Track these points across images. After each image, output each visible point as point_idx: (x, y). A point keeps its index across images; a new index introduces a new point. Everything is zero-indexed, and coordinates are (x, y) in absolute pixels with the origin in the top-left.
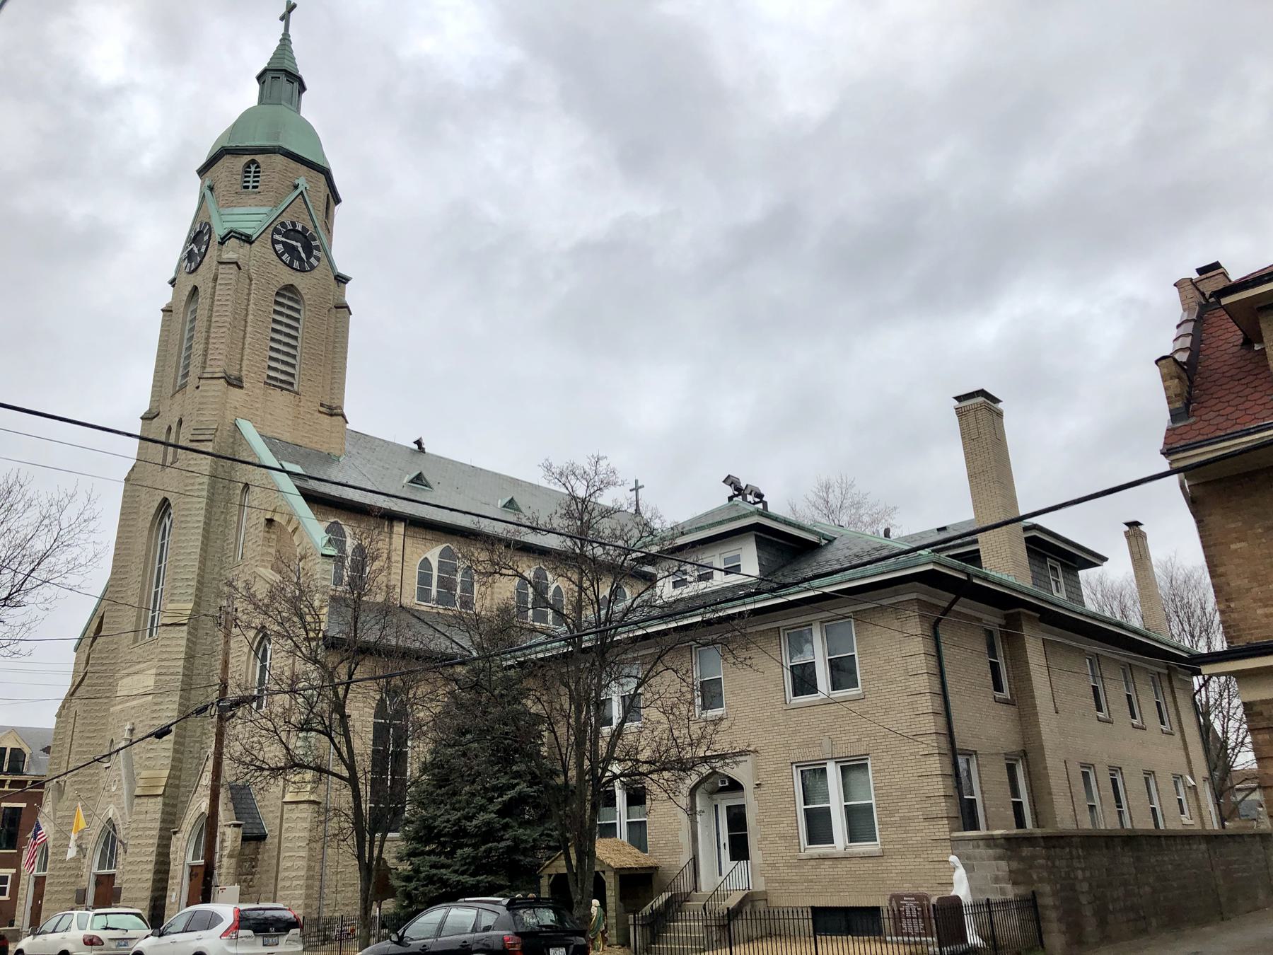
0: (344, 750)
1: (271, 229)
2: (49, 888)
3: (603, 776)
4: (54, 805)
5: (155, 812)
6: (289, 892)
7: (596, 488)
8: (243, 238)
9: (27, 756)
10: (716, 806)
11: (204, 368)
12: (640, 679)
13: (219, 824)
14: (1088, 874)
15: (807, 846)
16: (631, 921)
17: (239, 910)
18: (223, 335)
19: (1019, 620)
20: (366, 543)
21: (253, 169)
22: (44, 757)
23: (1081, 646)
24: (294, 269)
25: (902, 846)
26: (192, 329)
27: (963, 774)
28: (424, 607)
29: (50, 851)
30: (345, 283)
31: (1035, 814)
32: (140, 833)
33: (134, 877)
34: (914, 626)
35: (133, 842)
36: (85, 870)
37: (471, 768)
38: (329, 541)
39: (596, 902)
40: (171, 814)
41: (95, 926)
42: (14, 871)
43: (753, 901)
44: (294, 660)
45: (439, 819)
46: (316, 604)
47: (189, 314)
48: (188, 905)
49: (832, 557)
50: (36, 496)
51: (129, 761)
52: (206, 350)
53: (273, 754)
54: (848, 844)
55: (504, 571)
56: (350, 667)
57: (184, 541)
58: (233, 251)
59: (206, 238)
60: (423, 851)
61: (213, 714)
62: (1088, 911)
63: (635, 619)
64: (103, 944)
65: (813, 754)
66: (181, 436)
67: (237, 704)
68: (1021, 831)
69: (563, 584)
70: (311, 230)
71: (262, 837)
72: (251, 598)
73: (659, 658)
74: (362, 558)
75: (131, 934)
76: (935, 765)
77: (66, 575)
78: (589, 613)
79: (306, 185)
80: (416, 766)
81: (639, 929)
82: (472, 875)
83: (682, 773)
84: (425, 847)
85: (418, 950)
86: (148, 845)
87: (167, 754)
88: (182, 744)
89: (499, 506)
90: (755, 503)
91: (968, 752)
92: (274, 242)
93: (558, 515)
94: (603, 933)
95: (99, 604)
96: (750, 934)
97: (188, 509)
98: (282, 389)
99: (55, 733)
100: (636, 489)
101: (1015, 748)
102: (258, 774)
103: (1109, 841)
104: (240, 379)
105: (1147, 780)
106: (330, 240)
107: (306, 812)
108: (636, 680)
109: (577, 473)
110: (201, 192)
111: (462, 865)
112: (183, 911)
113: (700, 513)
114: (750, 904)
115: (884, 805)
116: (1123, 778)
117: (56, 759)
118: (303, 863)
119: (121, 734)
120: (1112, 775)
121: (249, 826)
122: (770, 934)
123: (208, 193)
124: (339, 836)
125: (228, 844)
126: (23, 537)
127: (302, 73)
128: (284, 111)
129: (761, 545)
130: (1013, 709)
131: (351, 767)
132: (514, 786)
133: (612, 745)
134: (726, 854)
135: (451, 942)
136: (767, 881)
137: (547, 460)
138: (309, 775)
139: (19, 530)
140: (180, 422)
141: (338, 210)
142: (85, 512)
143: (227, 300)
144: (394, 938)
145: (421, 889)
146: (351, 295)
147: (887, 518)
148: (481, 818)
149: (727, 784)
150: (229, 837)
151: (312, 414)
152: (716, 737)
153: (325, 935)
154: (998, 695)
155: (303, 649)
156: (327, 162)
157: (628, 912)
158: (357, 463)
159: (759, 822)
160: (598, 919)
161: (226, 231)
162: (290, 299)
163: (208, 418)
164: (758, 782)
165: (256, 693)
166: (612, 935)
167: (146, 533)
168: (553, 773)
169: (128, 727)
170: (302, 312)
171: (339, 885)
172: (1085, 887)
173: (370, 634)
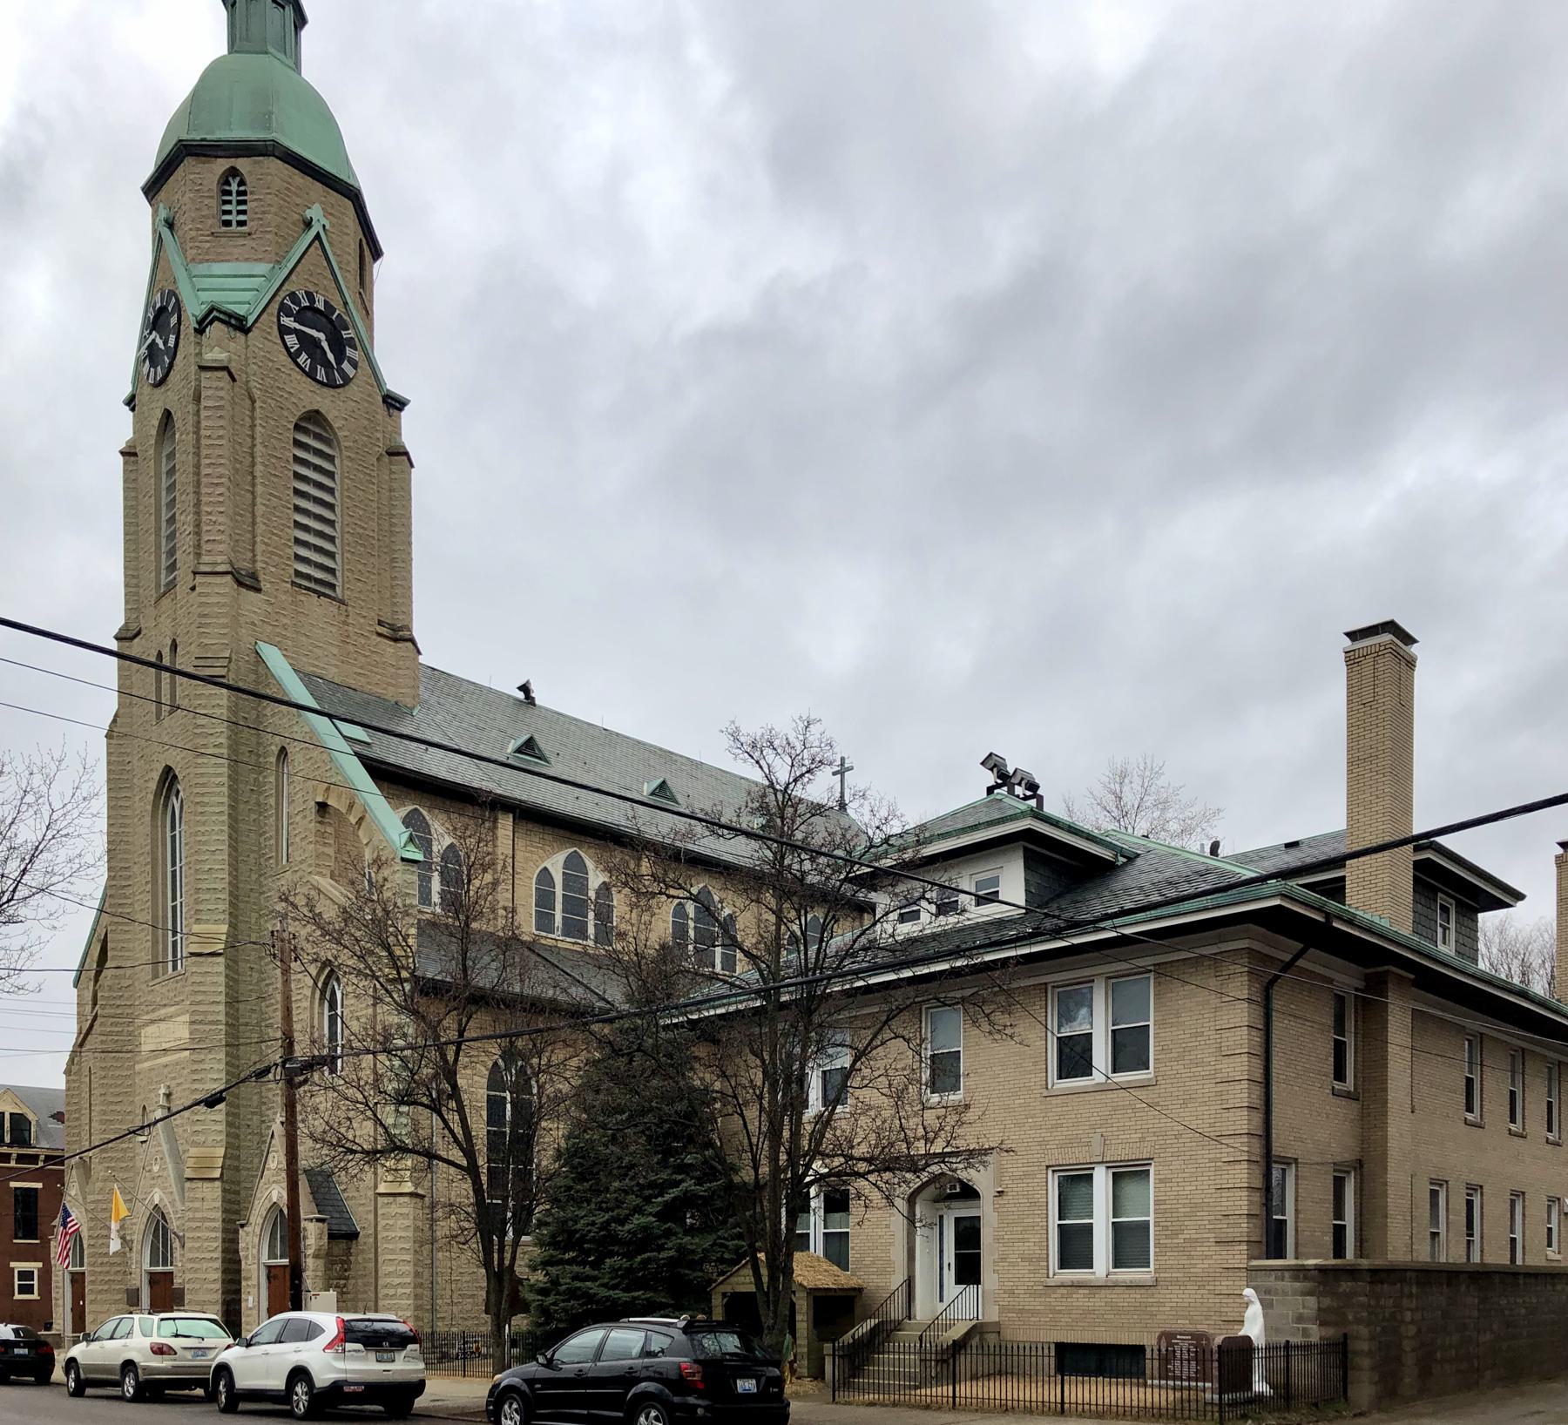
1: (275, 306)
2: (90, 1287)
3: (805, 1174)
4: (82, 1189)
7: (804, 769)
8: (233, 321)
9: (33, 1123)
10: (941, 1217)
11: (198, 555)
14: (1418, 1316)
15: (1057, 1271)
18: (221, 499)
19: (1386, 983)
21: (234, 187)
22: (54, 1125)
23: (1457, 1020)
25: (1182, 1275)
27: (1276, 1191)
30: (400, 410)
31: (1361, 1242)
32: (199, 1224)
34: (1240, 986)
35: (191, 1235)
36: (134, 1267)
38: (411, 839)
40: (233, 1203)
41: (162, 1333)
42: (40, 1265)
43: (982, 1333)
45: (582, 1221)
47: (164, 460)
48: (271, 1313)
49: (1134, 885)
51: (172, 1138)
53: (364, 1132)
54: (1111, 1270)
55: (672, 892)
57: (203, 834)
58: (219, 346)
59: (174, 320)
62: (1409, 1360)
63: (855, 966)
64: (176, 1354)
65: (1075, 1156)
67: (311, 1065)
68: (1338, 1261)
70: (336, 303)
71: (354, 1236)
72: (316, 919)
73: (886, 1022)
75: (207, 1343)
76: (1242, 1175)
77: (72, 879)
79: (324, 221)
82: (624, 1290)
85: (573, 1376)
88: (236, 1115)
89: (645, 794)
90: (1026, 798)
91: (1285, 1160)
92: (283, 330)
94: (791, 1363)
95: (97, 921)
97: (203, 785)
98: (320, 594)
101: (1348, 1157)
103: (1451, 1276)
104: (254, 576)
105: (1513, 1203)
106: (370, 328)
109: (776, 743)
110: (154, 231)
111: (612, 1279)
114: (978, 1337)
115: (1166, 1224)
116: (1482, 1199)
118: (409, 1268)
119: (155, 1100)
120: (1468, 1195)
121: (334, 1221)
122: (1000, 1371)
123: (166, 232)
128: (271, 64)
129: (1031, 862)
130: (1355, 1105)
131: (469, 1153)
132: (677, 1184)
134: (950, 1276)
135: (610, 1368)
136: (1002, 1310)
137: (733, 722)
140: (174, 646)
141: (381, 271)
142: (83, 786)
143: (220, 437)
145: (562, 1304)
146: (412, 430)
147: (1204, 825)
149: (958, 1190)
150: (313, 1235)
154: (1338, 1085)
155: (395, 996)
156: (354, 175)
157: (822, 1339)
159: (997, 1239)
161: (205, 308)
162: (317, 437)
164: (1000, 1189)
166: (803, 1366)
167: (148, 818)
169: (162, 1091)
170: (337, 461)
171: (454, 1296)
172: (1412, 1330)
173: (486, 976)
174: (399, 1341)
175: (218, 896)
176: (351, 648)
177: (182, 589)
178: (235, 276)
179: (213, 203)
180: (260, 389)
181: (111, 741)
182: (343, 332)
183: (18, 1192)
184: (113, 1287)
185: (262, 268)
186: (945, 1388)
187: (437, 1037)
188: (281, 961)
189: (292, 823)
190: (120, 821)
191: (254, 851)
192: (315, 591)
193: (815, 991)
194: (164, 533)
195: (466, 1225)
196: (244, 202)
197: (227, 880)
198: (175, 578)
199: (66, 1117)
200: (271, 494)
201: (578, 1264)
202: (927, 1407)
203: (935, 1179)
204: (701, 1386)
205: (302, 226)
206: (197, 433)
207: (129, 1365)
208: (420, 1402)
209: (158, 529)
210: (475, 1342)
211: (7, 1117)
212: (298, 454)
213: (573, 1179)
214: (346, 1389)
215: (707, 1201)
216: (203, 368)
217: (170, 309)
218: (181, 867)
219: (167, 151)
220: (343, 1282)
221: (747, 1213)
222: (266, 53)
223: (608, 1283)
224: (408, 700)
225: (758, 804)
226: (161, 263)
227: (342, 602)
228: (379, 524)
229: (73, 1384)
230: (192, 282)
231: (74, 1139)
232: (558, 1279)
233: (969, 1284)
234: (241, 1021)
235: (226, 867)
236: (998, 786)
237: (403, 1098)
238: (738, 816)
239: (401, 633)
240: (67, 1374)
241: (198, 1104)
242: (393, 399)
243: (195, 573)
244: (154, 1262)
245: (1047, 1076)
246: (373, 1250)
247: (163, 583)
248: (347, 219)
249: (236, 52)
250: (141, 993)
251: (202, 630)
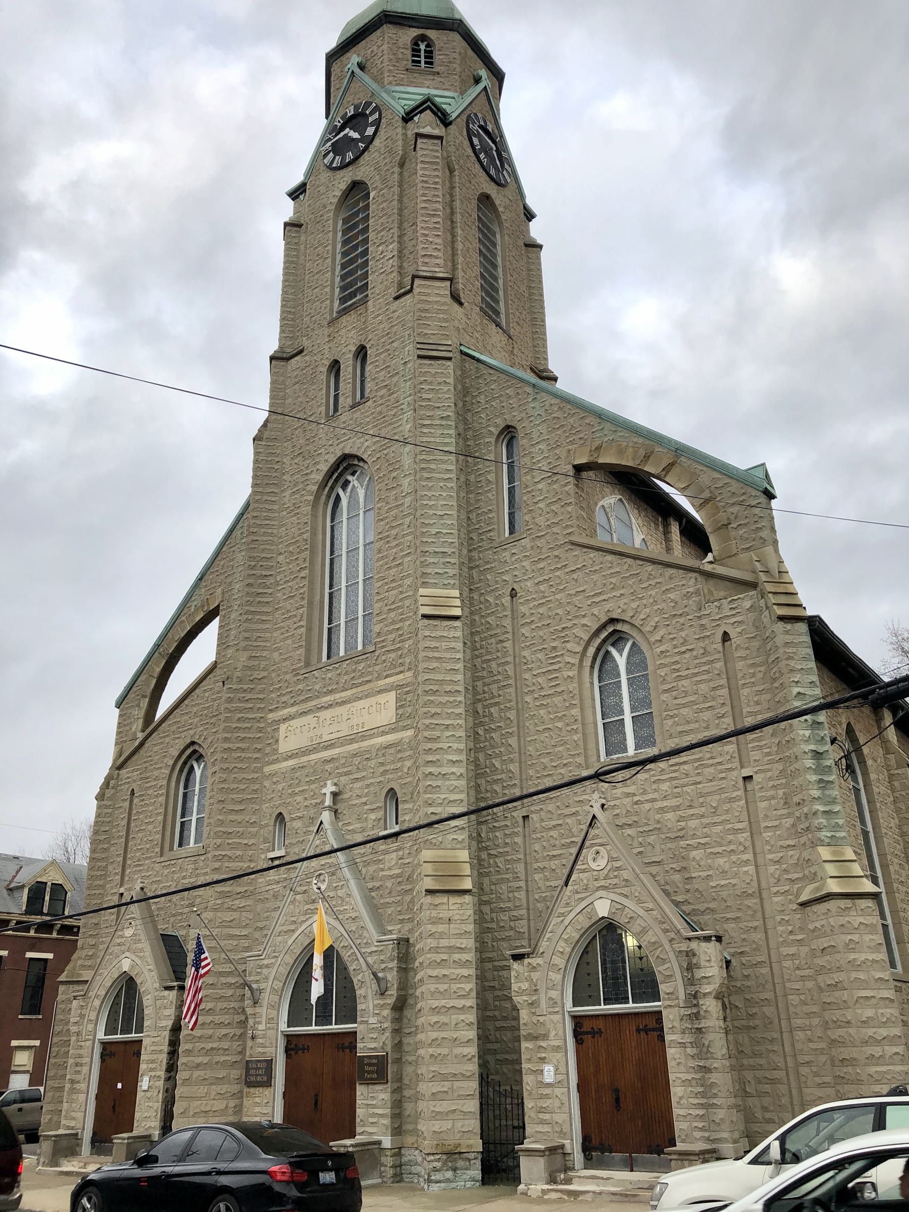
5: (463, 921)
8: (439, 114)
32: (445, 957)
57: (430, 499)
143: (436, 183)
169: (330, 788)
175: (448, 560)
184: (217, 1058)
205: (472, 81)
219: (344, 38)
231: (99, 873)
244: (110, 1030)
251: (421, 322)
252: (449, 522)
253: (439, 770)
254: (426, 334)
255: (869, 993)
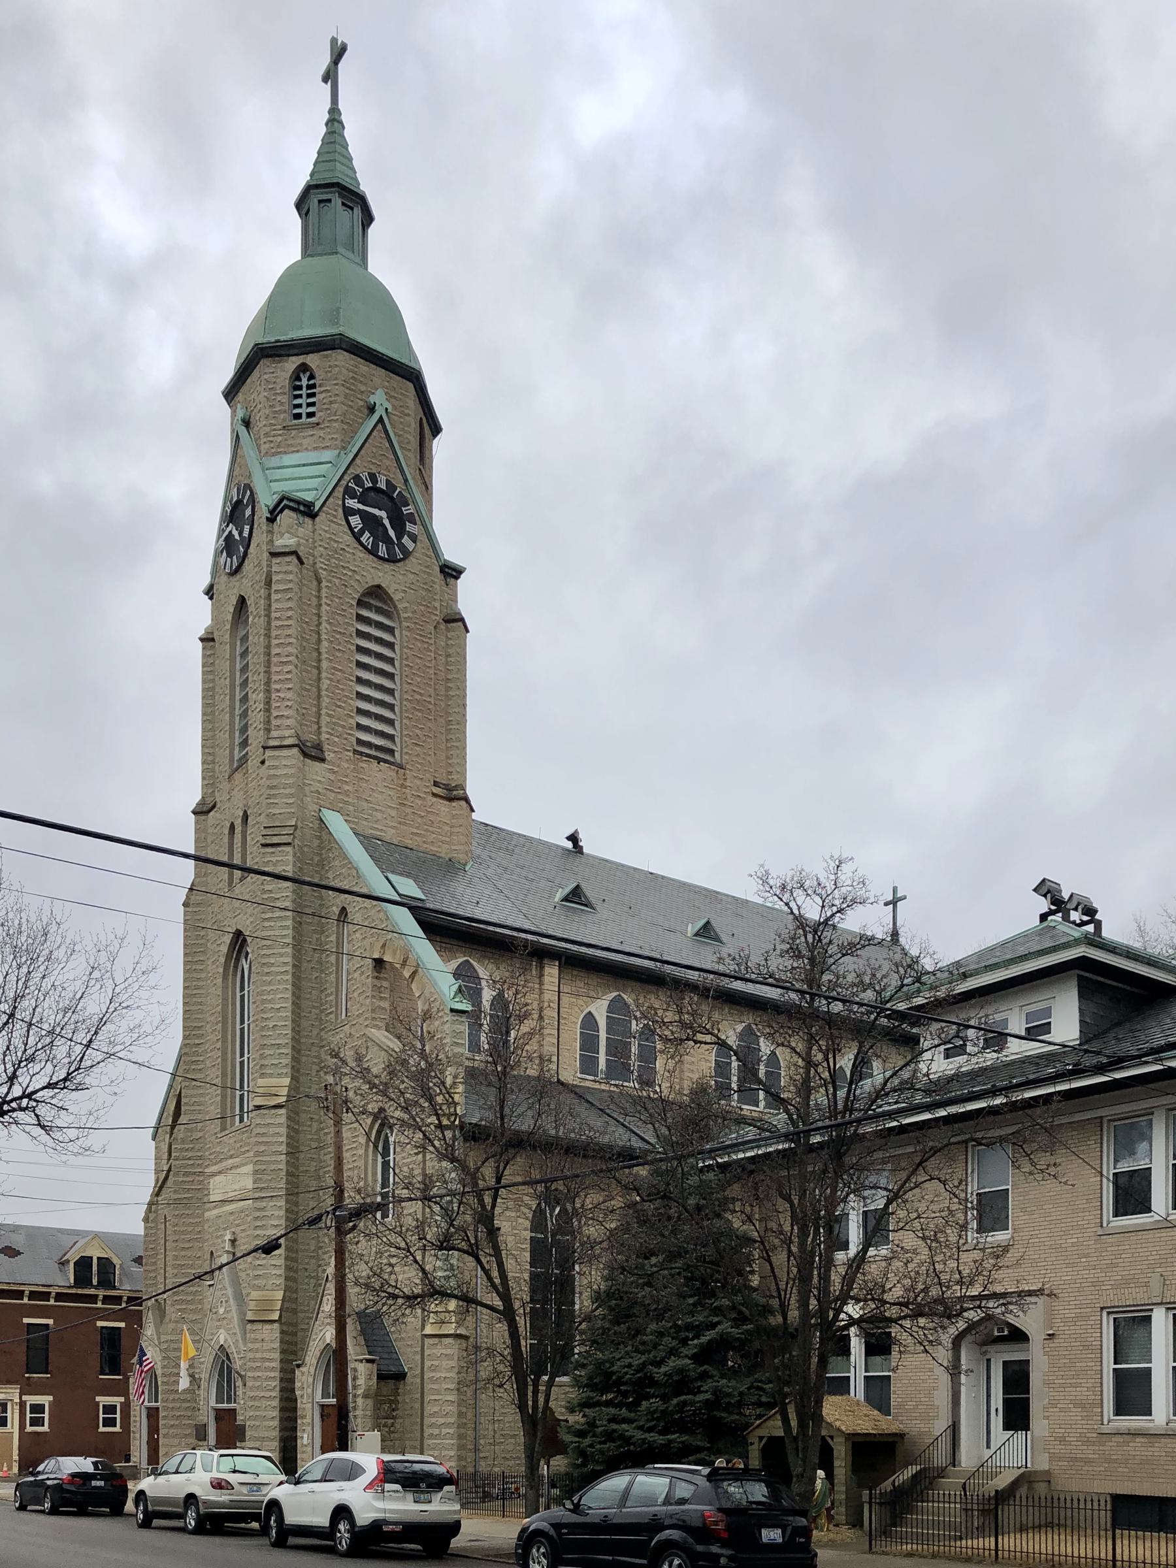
0: (495, 1274)
1: (341, 489)
2: (164, 1422)
3: (836, 1316)
5: (272, 1341)
6: (439, 1441)
7: (835, 909)
8: (302, 508)
9: (118, 1267)
10: (989, 1361)
11: (268, 730)
12: (890, 1191)
13: (349, 1358)
16: (866, 1498)
17: (383, 1461)
18: (289, 676)
20: (509, 995)
21: (304, 382)
22: (135, 1269)
24: (380, 558)
26: (244, 669)
28: (588, 1082)
29: (159, 1379)
30: (457, 578)
33: (258, 1413)
36: (202, 1403)
37: (658, 1302)
38: (460, 990)
39: (821, 1473)
40: (291, 1344)
41: (221, 1469)
42: (122, 1399)
44: (424, 1156)
46: (449, 1081)
48: (324, 1450)
50: (78, 939)
51: (236, 1283)
52: (268, 703)
53: (407, 1278)
55: (699, 1037)
56: (498, 1167)
59: (248, 512)
60: (598, 1401)
61: (329, 1224)
65: (1132, 1297)
66: (248, 838)
67: (359, 1213)
69: (783, 1054)
71: (401, 1376)
73: (920, 1164)
74: (504, 1018)
77: (131, 1048)
78: (820, 1098)
80: (586, 1294)
81: (875, 1508)
82: (661, 1433)
83: (945, 1320)
84: (602, 1396)
85: (597, 1521)
86: (268, 1379)
87: (278, 1272)
88: (295, 1260)
89: (689, 935)
90: (1083, 923)
92: (348, 512)
93: (778, 952)
94: (828, 1510)
96: (1024, 1522)
98: (379, 760)
99: (145, 1241)
100: (894, 902)
102: (390, 1302)
104: (319, 747)
107: (451, 1348)
108: (885, 1193)
110: (233, 430)
111: (648, 1421)
112: (319, 1458)
113: (991, 942)
117: (150, 1272)
118: (453, 1409)
123: (243, 431)
124: (492, 1381)
125: (361, 1381)
126: (71, 995)
127: (367, 186)
128: (342, 263)
131: (506, 1297)
132: (713, 1326)
133: (849, 1280)
134: (997, 1421)
138: (452, 1304)
139: (65, 985)
140: (245, 817)
141: (440, 447)
142: (142, 961)
143: (289, 618)
144: (569, 1505)
148: (671, 1364)
149: (1006, 1333)
150: (362, 1375)
151: (424, 799)
152: (996, 1275)
153: (484, 1492)
155: (436, 1143)
157: (861, 1486)
158: (489, 872)
160: (824, 1494)
161: (276, 498)
162: (379, 611)
163: (284, 809)
165: (379, 1199)
166: (840, 1513)
167: (220, 981)
168: (767, 1310)
169: (228, 1237)
170: (397, 632)
171: (497, 1436)
174: (436, 1482)
175: (282, 1051)
176: (408, 810)
177: (253, 763)
178: (304, 465)
179: (284, 399)
180: (325, 570)
181: (187, 909)
182: (403, 509)
183: (104, 1331)
185: (328, 455)
186: (987, 1540)
187: (476, 1184)
188: (334, 1113)
189: (351, 980)
190: (194, 983)
191: (314, 1007)
192: (375, 758)
193: (845, 1133)
194: (237, 712)
195: (501, 1368)
196: (313, 395)
197: (290, 1036)
198: (247, 753)
199: (144, 1260)
200: (334, 668)
201: (616, 1406)
202: (968, 1560)
203: (972, 1327)
204: (725, 1535)
205: (366, 411)
206: (268, 616)
207: (191, 1498)
208: (456, 1543)
209: (232, 708)
210: (515, 1482)
211: (95, 1261)
212: (359, 628)
213: (611, 1322)
214: (385, 1528)
215: (743, 1343)
216: (274, 555)
217: (245, 501)
218: (249, 1025)
220: (390, 1421)
221: (776, 1361)
222: (337, 253)
223: (643, 1426)
224: (461, 856)
225: (788, 946)
226: (238, 460)
227: (401, 767)
228: (435, 689)
229: (141, 1516)
230: (265, 475)
232: (595, 1420)
233: (1017, 1431)
234: (301, 1169)
235: (289, 1023)
236: (1052, 913)
237: (442, 1244)
238: (766, 960)
239: (455, 792)
240: (137, 1506)
241: (255, 1250)
242: (449, 568)
243: (265, 748)
245: (1101, 1214)
246: (419, 1390)
247: (236, 758)
248: (407, 400)
249: (309, 256)
250: (211, 1145)
252: (284, 1015)
253: (264, 1232)
254: (274, 815)
255: (437, 1397)
